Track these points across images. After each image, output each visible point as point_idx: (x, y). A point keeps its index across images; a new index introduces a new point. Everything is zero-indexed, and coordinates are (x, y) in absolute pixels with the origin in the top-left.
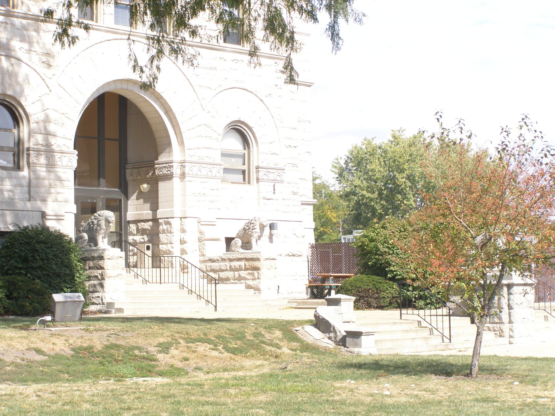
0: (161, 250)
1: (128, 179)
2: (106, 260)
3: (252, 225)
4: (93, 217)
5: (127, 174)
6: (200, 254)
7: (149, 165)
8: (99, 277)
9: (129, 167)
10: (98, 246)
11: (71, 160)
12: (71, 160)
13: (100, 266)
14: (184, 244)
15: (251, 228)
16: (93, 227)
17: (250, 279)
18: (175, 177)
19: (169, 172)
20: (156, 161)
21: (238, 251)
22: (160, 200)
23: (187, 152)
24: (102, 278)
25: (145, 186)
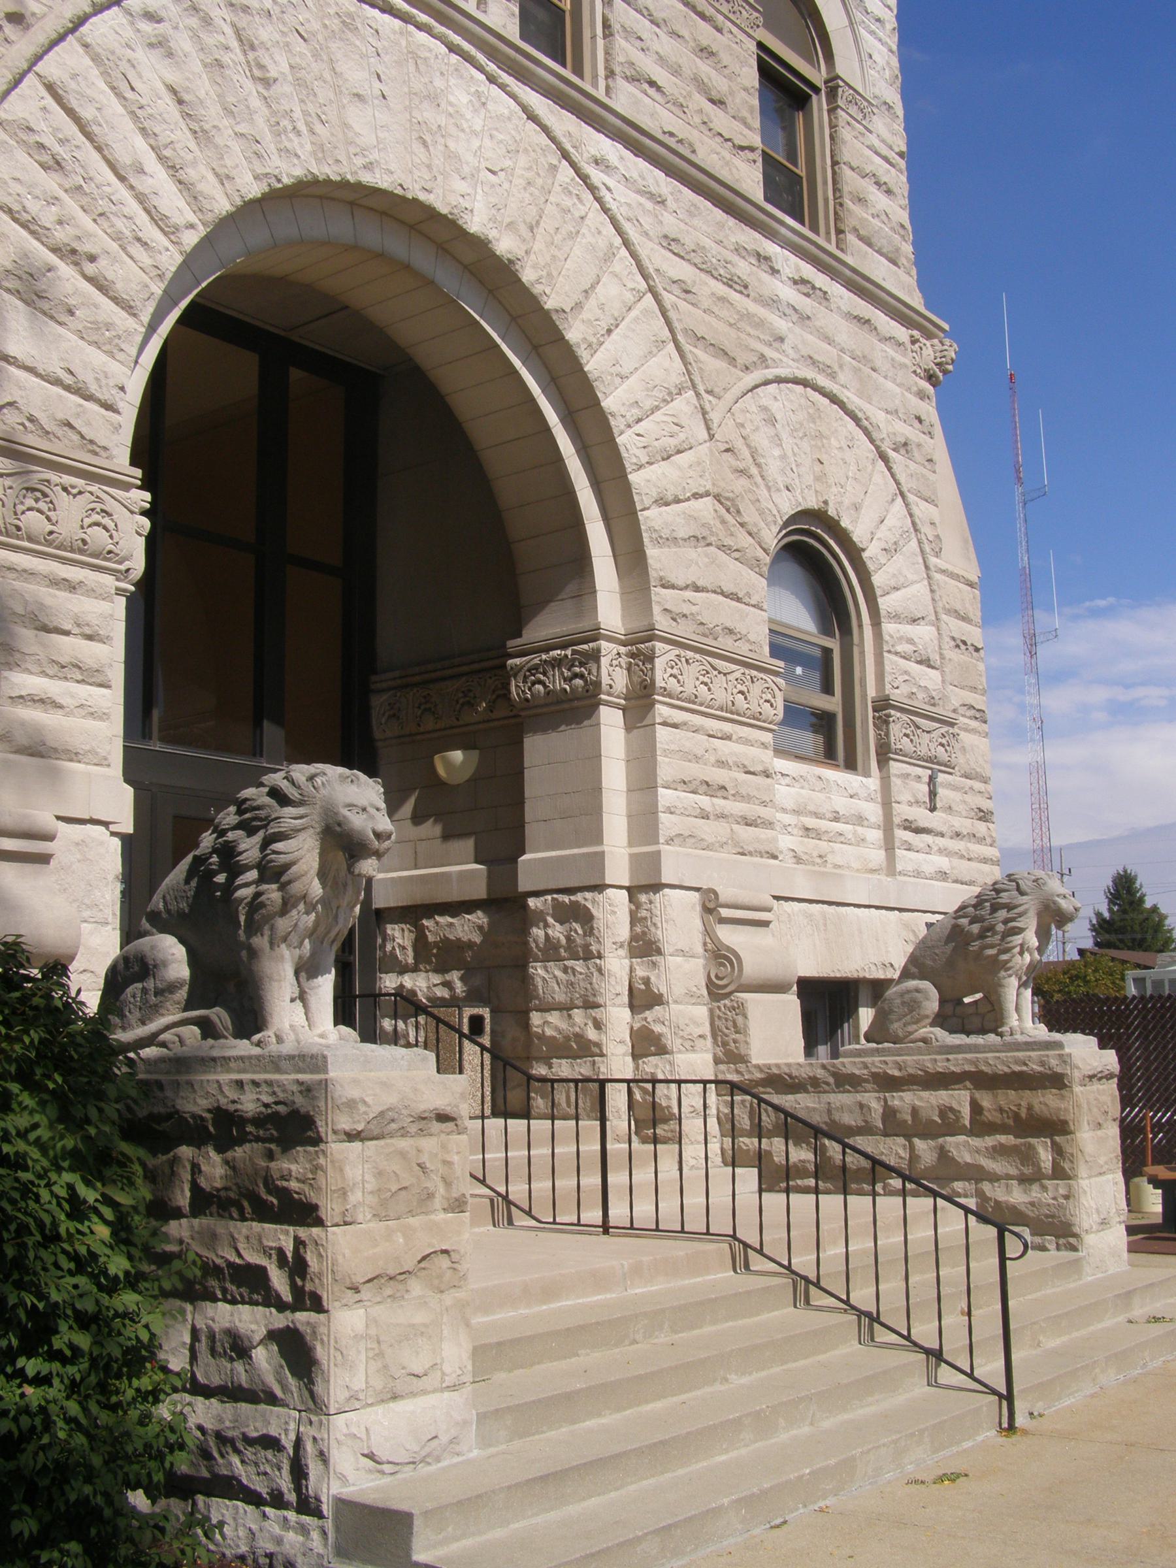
0: (542, 1037)
1: (377, 734)
2: (336, 1148)
3: (1002, 914)
4: (229, 817)
5: (374, 713)
6: (720, 1051)
7: (476, 666)
8: (279, 1281)
9: (384, 685)
10: (268, 1034)
11: (106, 521)
12: (106, 521)
13: (284, 1194)
14: (649, 1007)
15: (1000, 927)
16: (229, 888)
17: (1009, 1177)
18: (608, 704)
19: (578, 682)
20: (511, 643)
21: (925, 1040)
22: (531, 811)
23: (659, 595)
24: (297, 1292)
25: (457, 756)
